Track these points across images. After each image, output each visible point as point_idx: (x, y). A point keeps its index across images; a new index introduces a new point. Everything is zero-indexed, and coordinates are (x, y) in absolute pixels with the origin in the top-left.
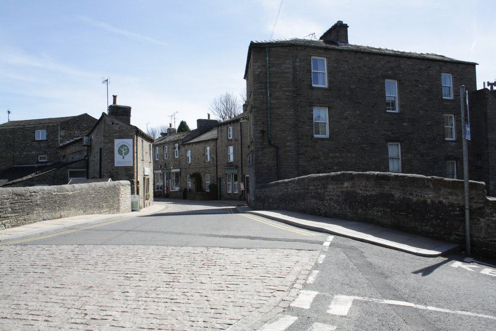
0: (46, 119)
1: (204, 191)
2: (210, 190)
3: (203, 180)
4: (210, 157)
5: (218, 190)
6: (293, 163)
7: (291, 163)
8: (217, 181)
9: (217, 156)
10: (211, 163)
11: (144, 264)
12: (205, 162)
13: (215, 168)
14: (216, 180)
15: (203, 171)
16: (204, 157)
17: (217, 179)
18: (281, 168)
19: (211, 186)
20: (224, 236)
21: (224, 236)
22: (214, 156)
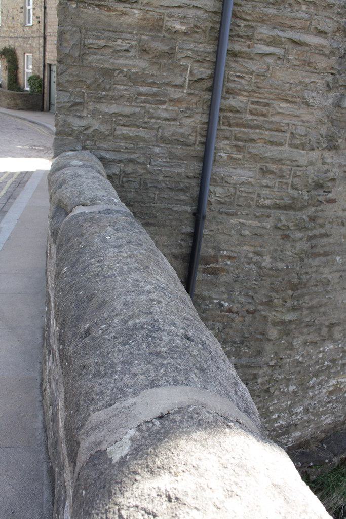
0: (35, 157)
1: (20, 89)
2: (31, 88)
3: (20, 66)
4: (34, 14)
5: (46, 91)
6: (321, 33)
7: (305, 29)
8: (44, 70)
9: (45, 13)
10: (35, 28)
11: (331, 240)
12: (24, 26)
13: (41, 41)
14: (42, 69)
15: (20, 46)
16: (22, 15)
17: (44, 66)
18: (234, 54)
19: (33, 80)
20: (31, 121)
21: (31, 121)
22: (41, 15)
